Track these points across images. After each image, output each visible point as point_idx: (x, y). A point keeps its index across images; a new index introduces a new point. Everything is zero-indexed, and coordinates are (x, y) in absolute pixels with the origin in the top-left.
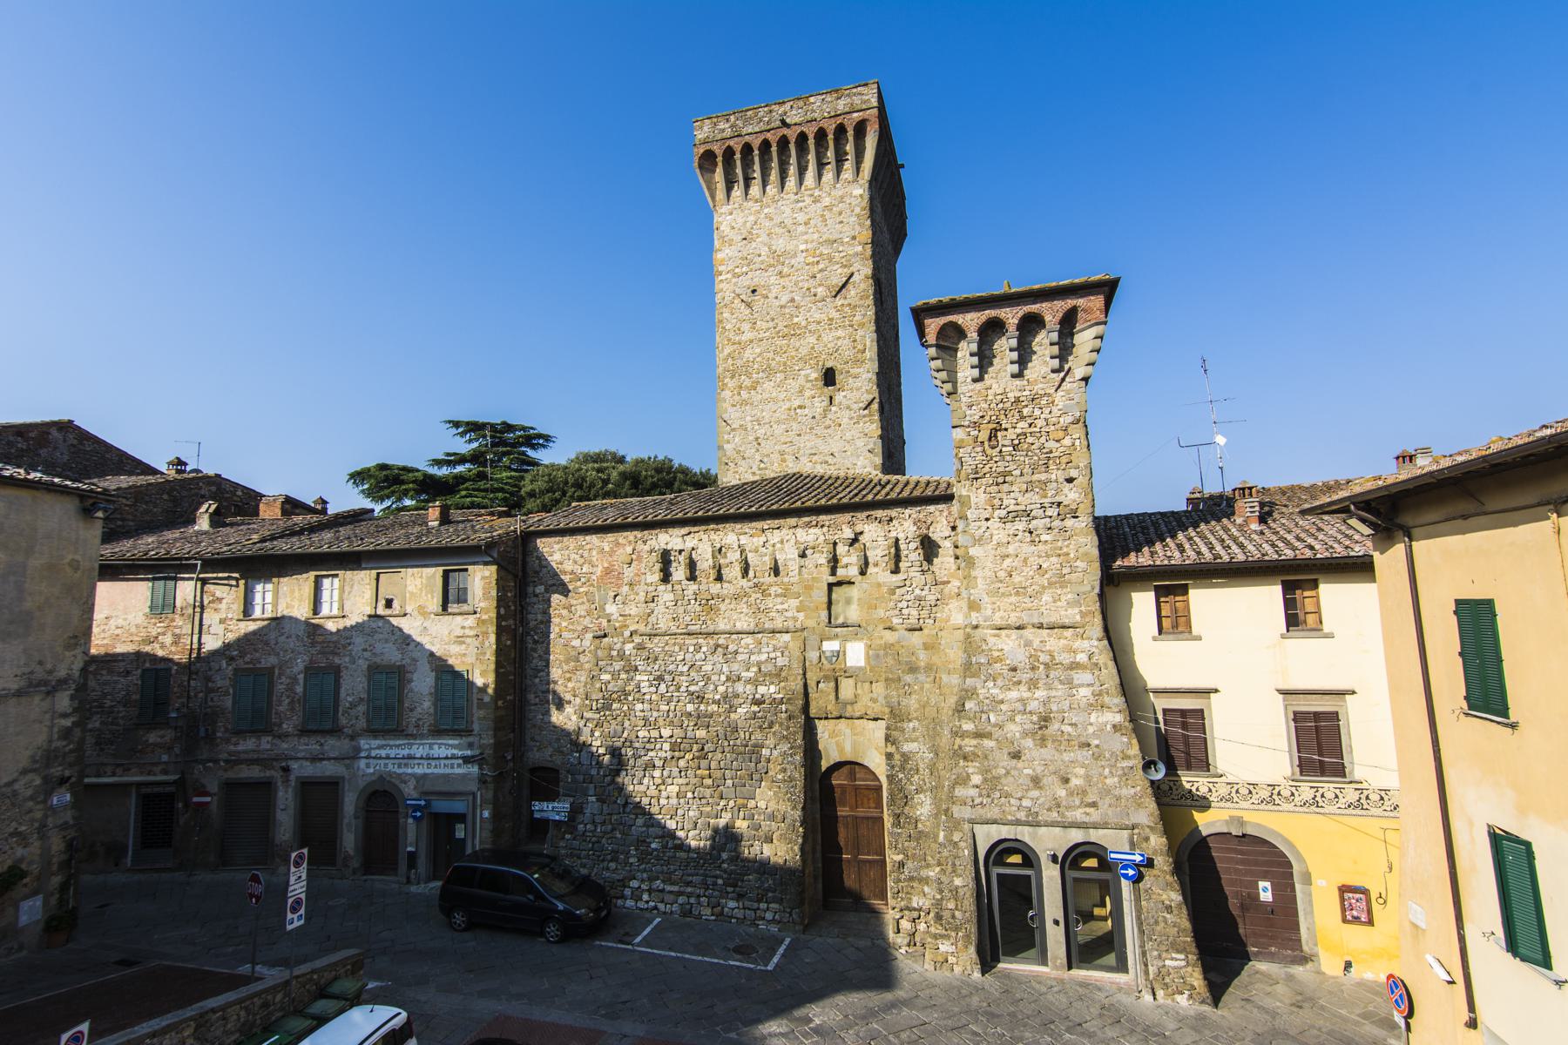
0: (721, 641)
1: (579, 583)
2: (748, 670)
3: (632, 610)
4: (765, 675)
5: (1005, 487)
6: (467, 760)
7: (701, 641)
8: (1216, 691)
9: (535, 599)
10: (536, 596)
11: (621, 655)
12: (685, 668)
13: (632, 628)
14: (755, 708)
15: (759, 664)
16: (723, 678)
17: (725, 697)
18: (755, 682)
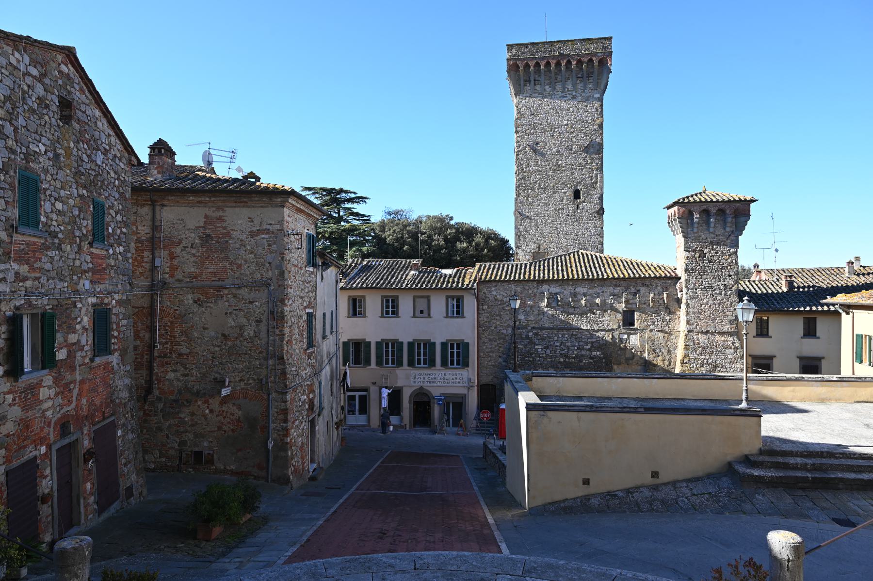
0: (575, 333)
1: (505, 305)
2: (587, 345)
3: (532, 318)
4: (595, 348)
5: (704, 277)
6: (507, 381)
7: (565, 332)
8: (823, 358)
9: (483, 312)
10: (484, 310)
11: (527, 337)
12: (558, 344)
13: (532, 326)
14: (591, 361)
15: (592, 343)
16: (576, 348)
17: (577, 356)
18: (590, 350)
